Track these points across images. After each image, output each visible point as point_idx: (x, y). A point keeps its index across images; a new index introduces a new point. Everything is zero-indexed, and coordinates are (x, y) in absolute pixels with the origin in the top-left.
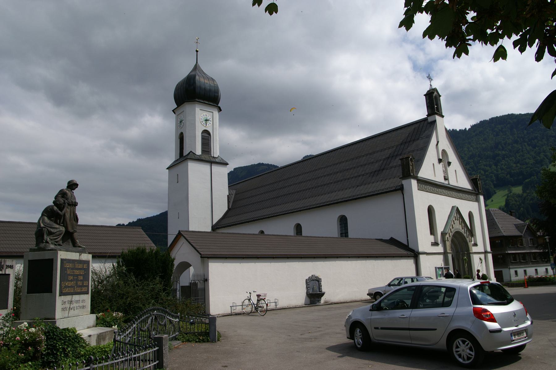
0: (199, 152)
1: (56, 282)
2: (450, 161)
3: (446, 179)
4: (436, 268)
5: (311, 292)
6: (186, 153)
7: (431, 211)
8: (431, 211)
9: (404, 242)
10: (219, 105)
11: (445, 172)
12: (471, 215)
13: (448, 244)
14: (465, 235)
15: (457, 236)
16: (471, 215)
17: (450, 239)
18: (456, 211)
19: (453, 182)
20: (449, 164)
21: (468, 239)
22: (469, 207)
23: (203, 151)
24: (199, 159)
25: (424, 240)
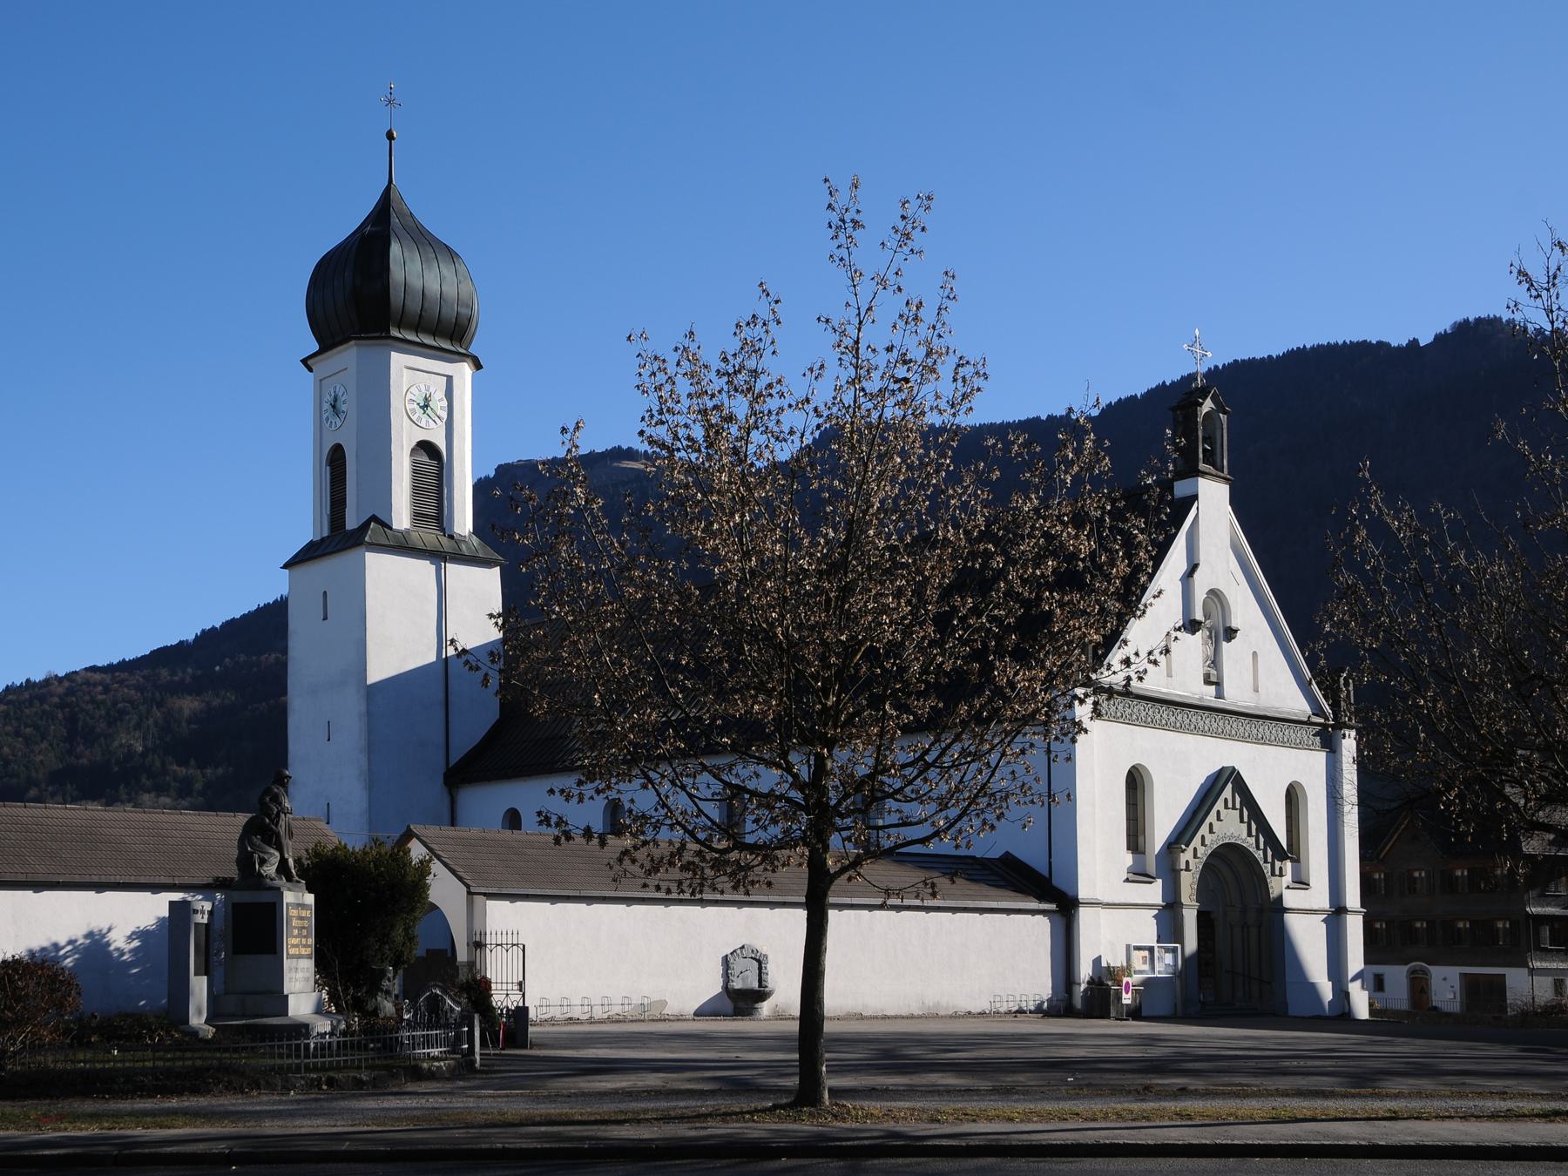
0: (402, 518)
1: (464, 511)
2: (1234, 625)
3: (1213, 680)
4: (1128, 947)
5: (1377, 1006)
6: (351, 523)
7: (1136, 782)
8: (1136, 782)
9: (1038, 862)
10: (473, 350)
11: (1215, 661)
12: (1293, 797)
13: (1188, 883)
14: (1259, 855)
15: (1227, 858)
16: (1293, 797)
17: (1196, 866)
18: (1225, 782)
19: (1237, 694)
20: (1230, 633)
21: (1267, 868)
22: (1309, 767)
23: (417, 516)
24: (403, 547)
25: (1099, 859)
